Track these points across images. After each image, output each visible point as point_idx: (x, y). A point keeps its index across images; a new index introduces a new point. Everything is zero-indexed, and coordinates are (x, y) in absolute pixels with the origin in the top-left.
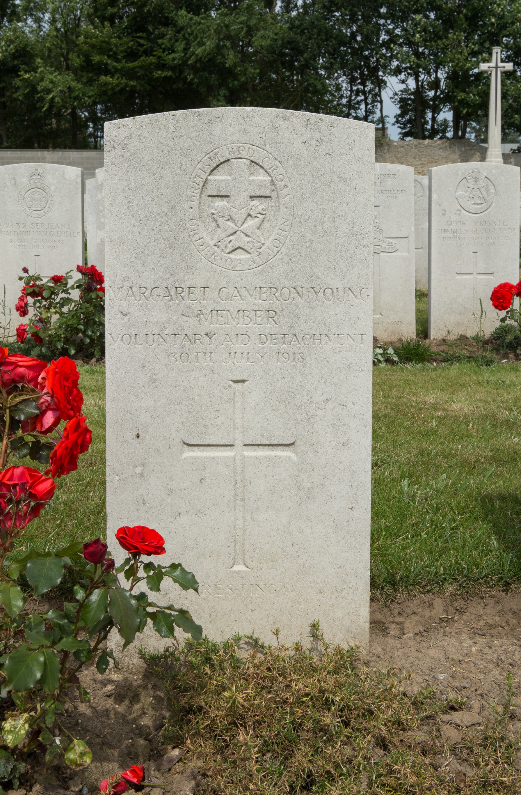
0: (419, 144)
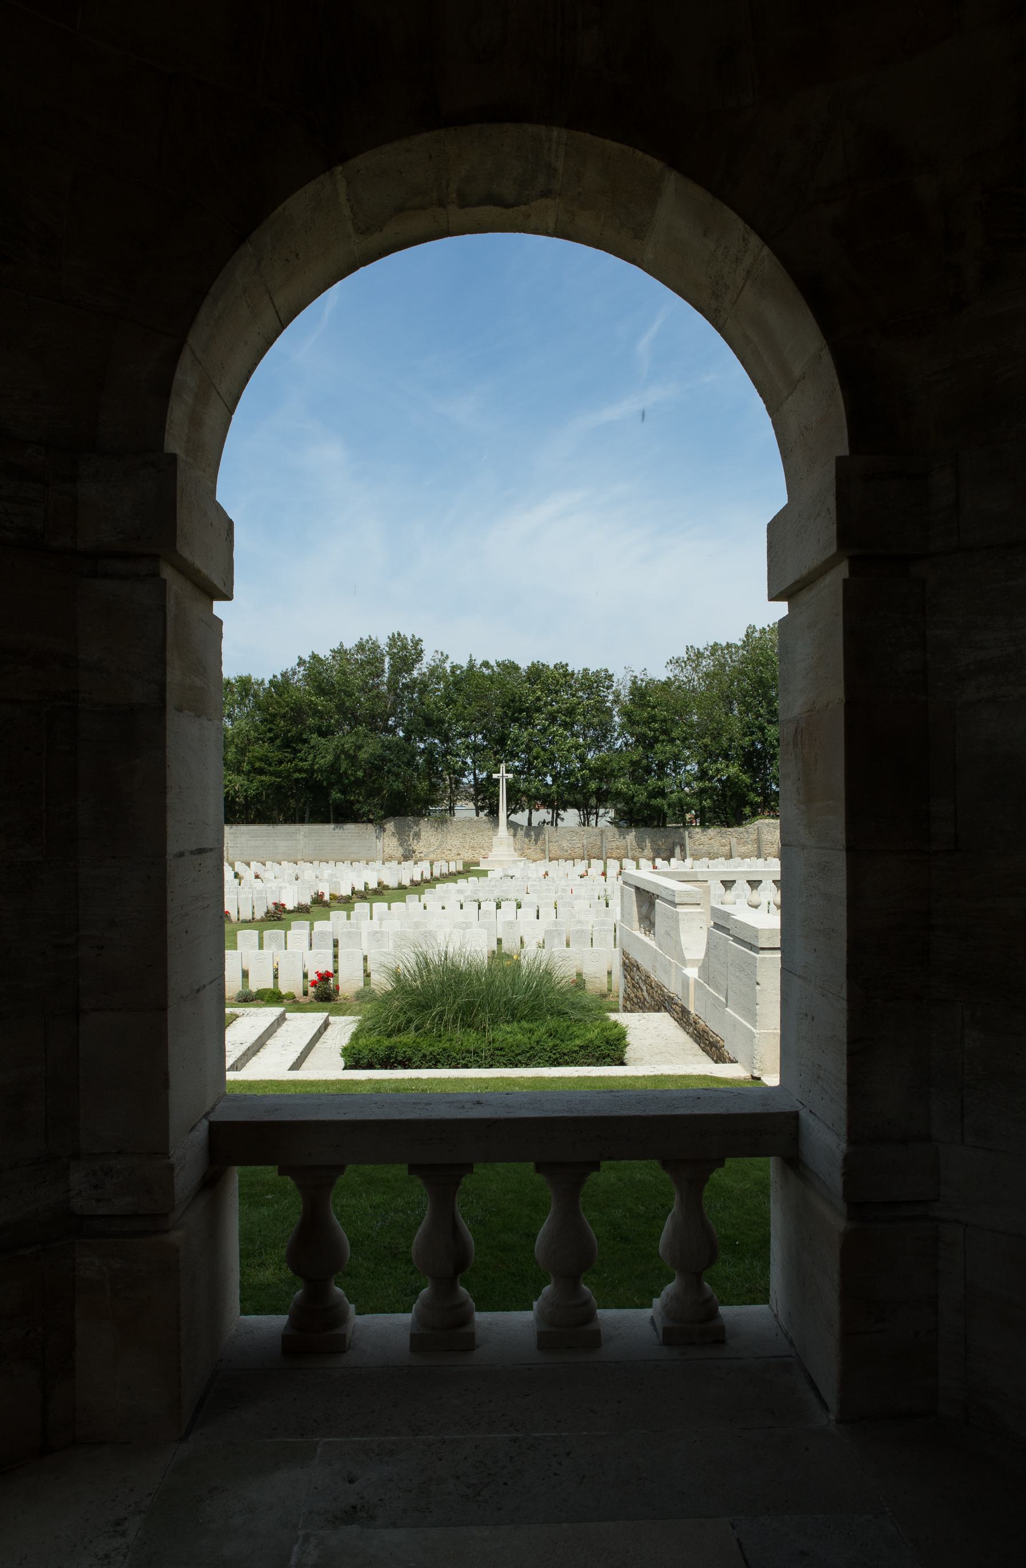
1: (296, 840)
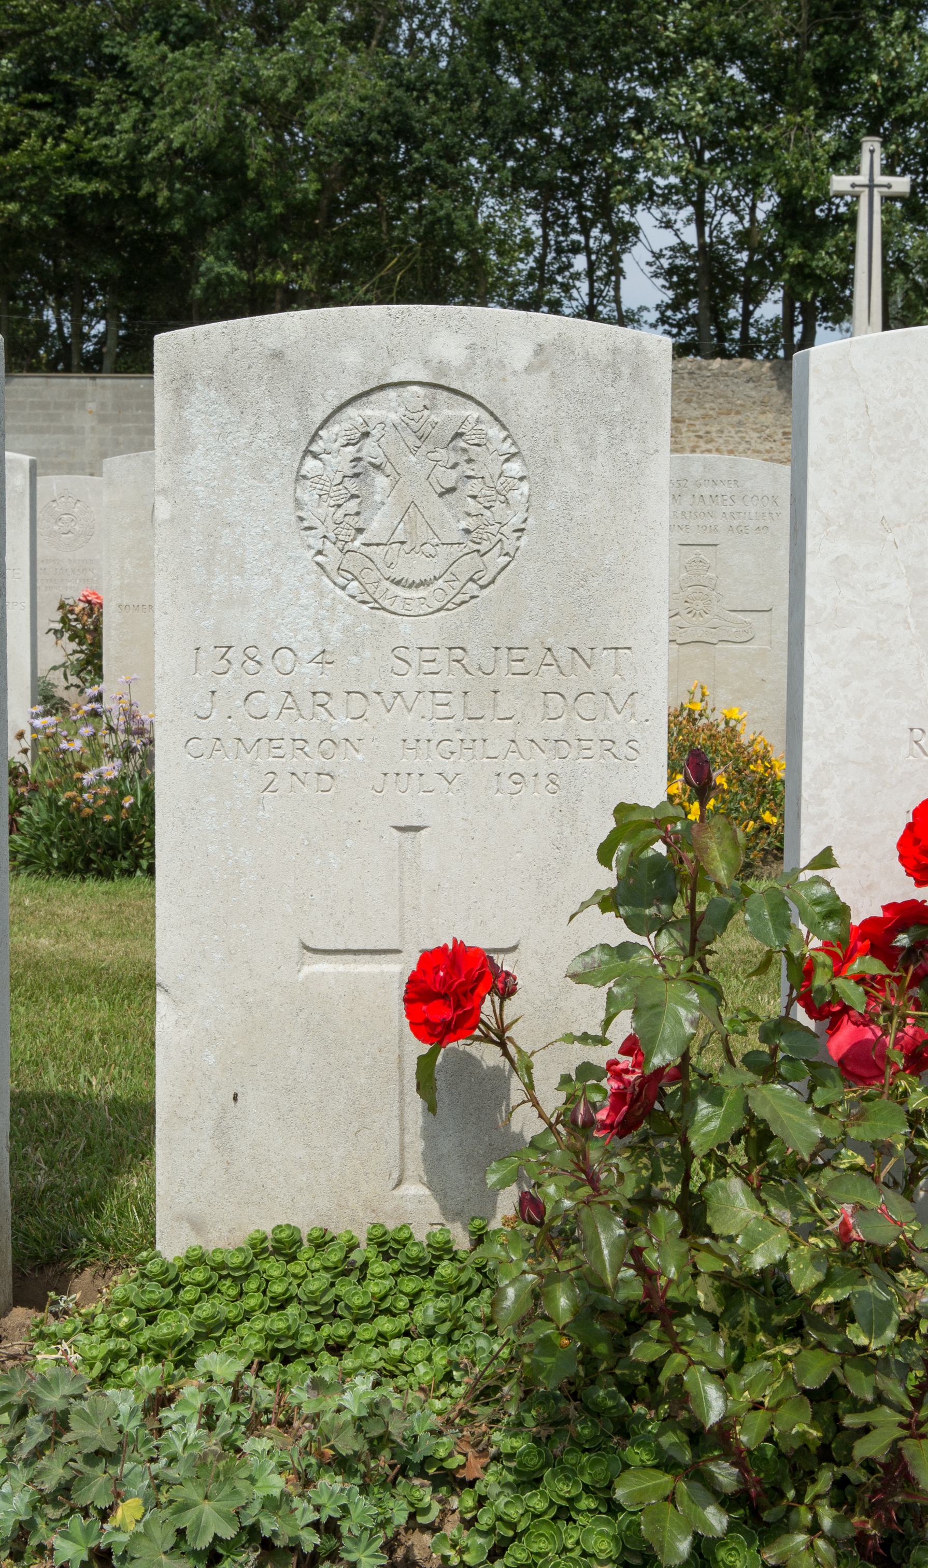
0: (700, 368)
1: (69, 430)
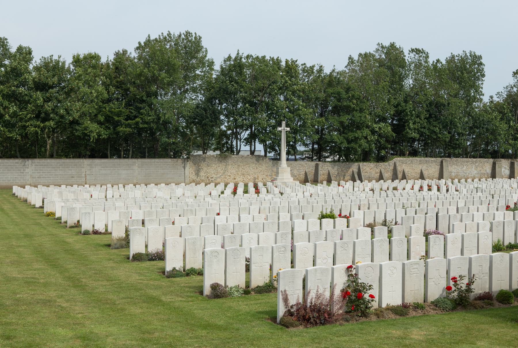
1: (133, 169)
